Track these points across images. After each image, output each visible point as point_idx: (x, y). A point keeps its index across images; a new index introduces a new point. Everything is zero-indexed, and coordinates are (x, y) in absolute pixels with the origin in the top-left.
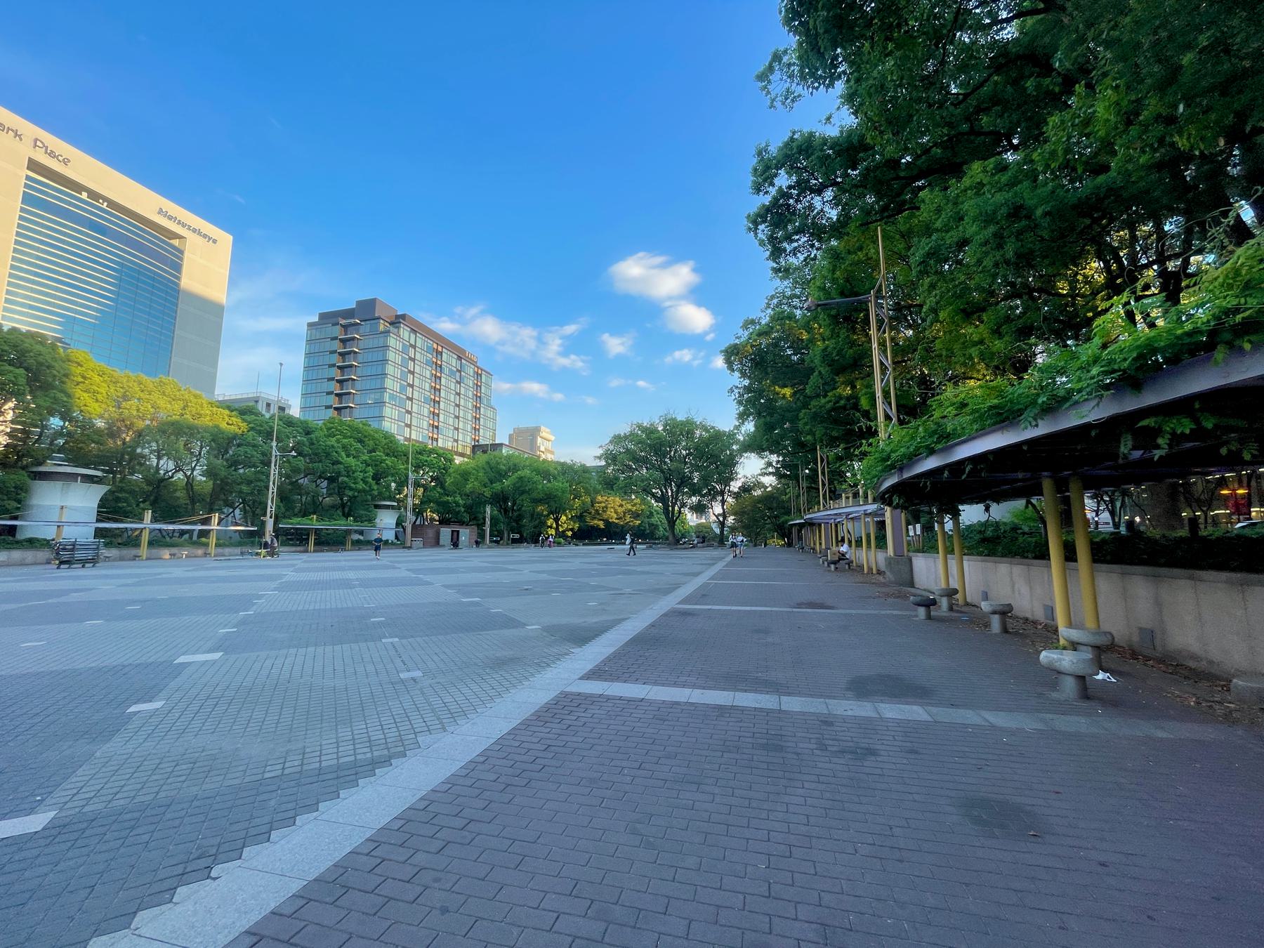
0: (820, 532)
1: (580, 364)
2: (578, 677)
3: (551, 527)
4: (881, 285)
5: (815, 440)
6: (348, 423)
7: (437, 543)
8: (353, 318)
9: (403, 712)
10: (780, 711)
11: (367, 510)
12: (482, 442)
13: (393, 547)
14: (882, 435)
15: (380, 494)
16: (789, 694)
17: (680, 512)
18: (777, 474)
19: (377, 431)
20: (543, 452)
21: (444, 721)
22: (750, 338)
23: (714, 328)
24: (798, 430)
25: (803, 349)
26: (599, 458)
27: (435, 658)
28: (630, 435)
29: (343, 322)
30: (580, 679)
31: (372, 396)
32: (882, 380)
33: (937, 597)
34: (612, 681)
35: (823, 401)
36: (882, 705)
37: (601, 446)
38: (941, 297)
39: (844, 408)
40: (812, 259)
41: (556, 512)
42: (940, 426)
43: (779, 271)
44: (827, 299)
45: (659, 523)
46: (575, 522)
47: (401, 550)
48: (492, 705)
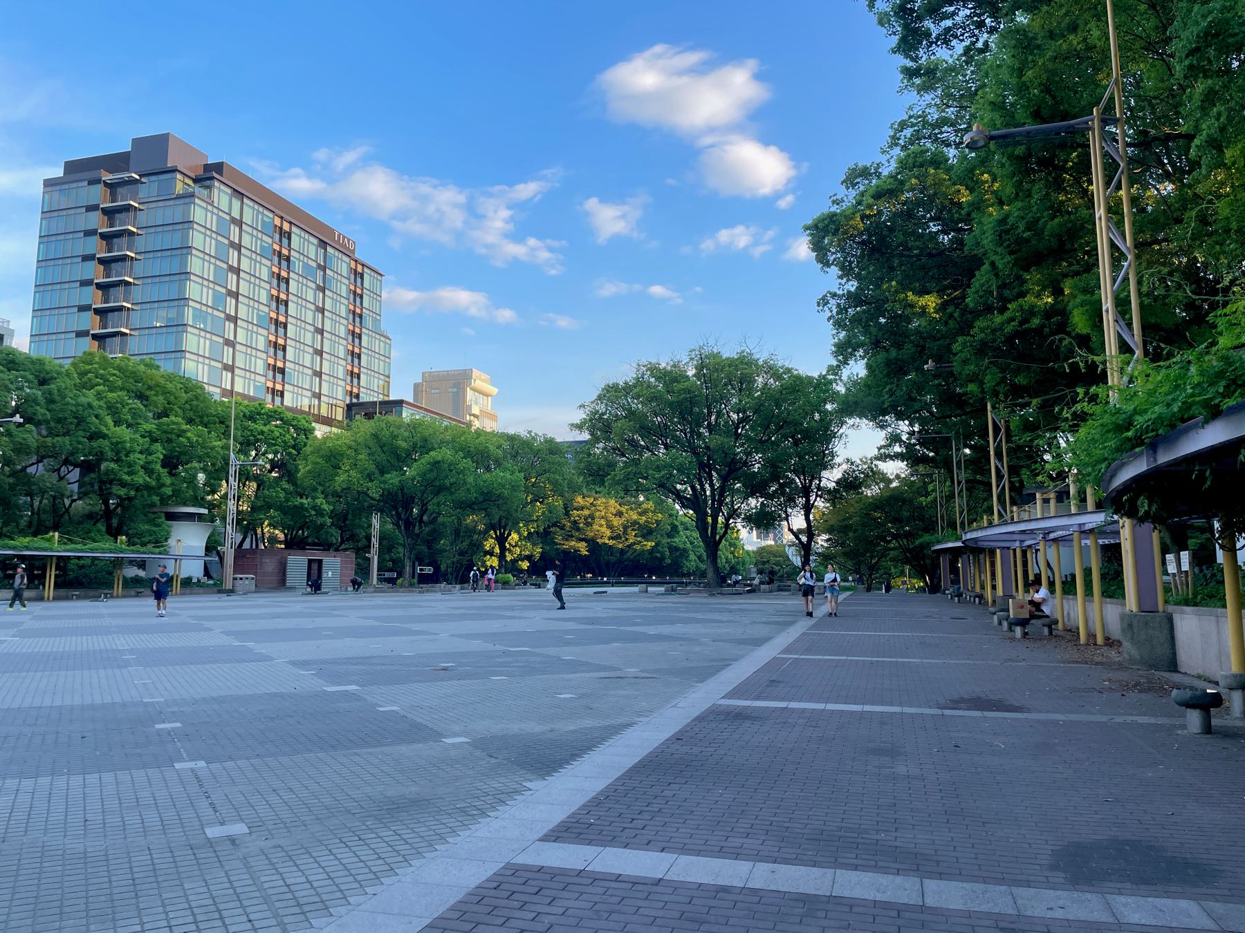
0: (993, 564)
1: (544, 255)
2: (541, 835)
3: (491, 553)
4: (1112, 98)
5: (983, 391)
6: (118, 361)
7: (281, 583)
8: (128, 170)
9: (210, 902)
10: (923, 908)
11: (152, 522)
12: (364, 398)
13: (201, 590)
14: (1113, 379)
15: (176, 493)
16: (941, 876)
17: (727, 526)
18: (910, 457)
19: (170, 378)
20: (475, 416)
21: (286, 920)
22: (859, 203)
23: (797, 185)
24: (952, 374)
25: (961, 221)
26: (579, 427)
27: (274, 799)
28: (635, 386)
29: (108, 177)
30: (545, 839)
31: (162, 313)
32: (1114, 280)
33: (1224, 692)
34: (603, 844)
35: (998, 319)
36: (1122, 899)
37: (582, 406)
38: (1230, 119)
39: (1039, 331)
40: (981, 51)
41: (501, 529)
42: (1230, 364)
43: (924, 76)
44: (1007, 125)
45: (688, 545)
46: (534, 545)
47: (215, 597)
48: (378, 889)
